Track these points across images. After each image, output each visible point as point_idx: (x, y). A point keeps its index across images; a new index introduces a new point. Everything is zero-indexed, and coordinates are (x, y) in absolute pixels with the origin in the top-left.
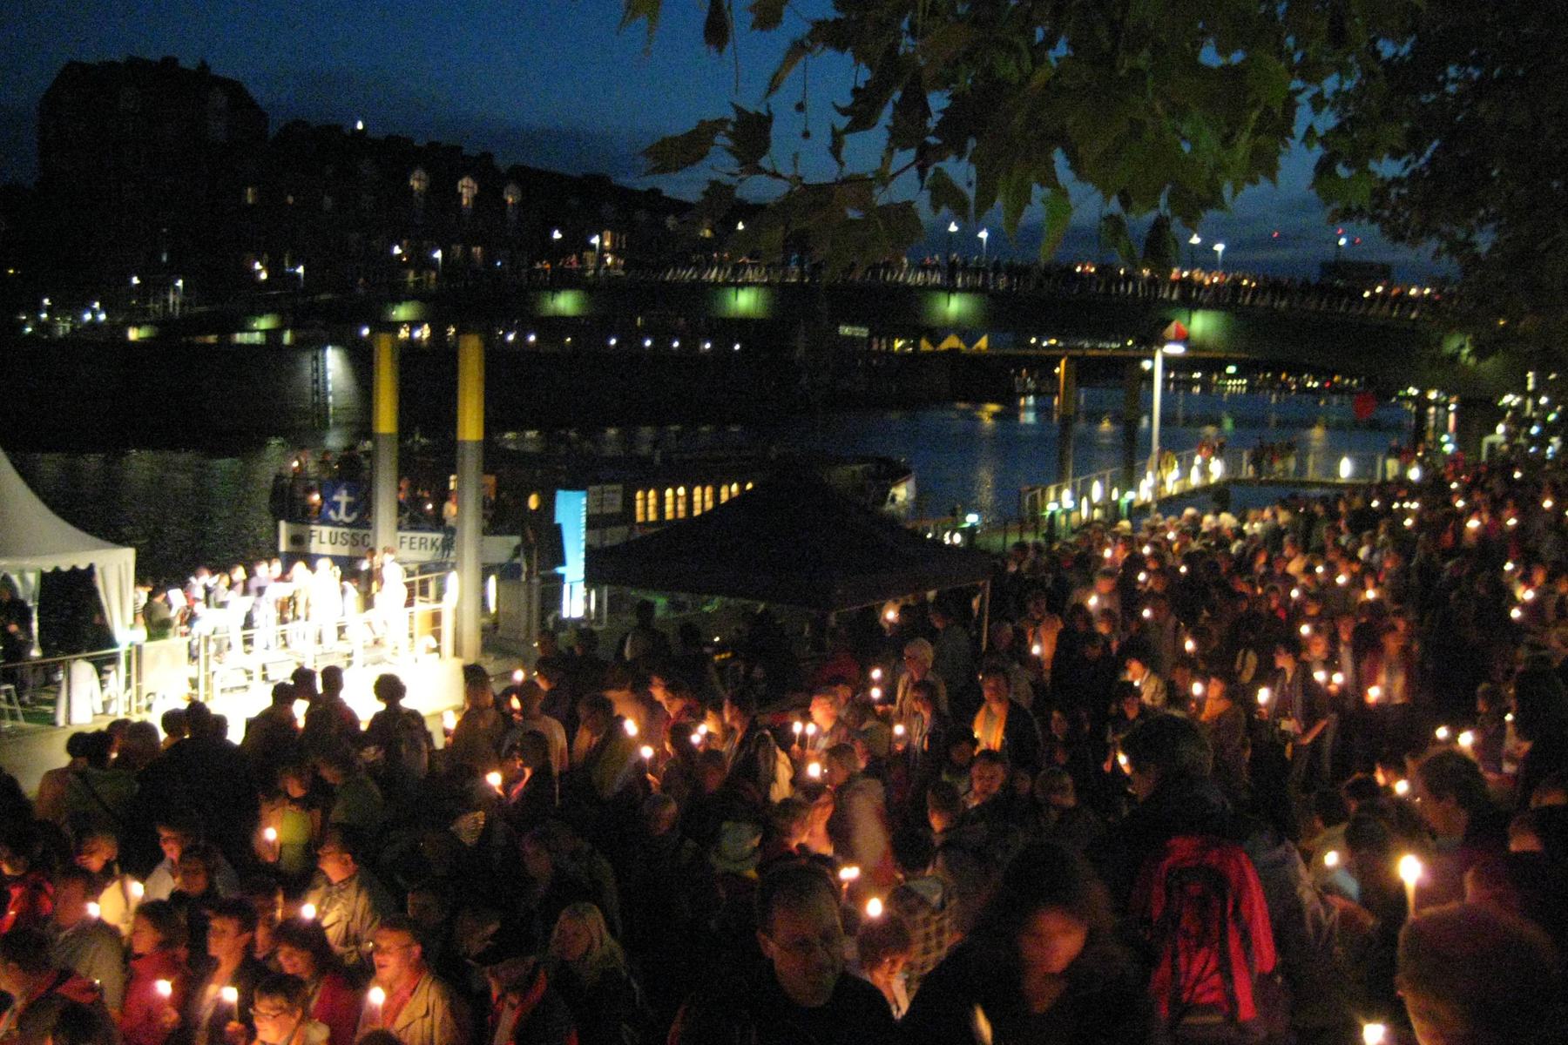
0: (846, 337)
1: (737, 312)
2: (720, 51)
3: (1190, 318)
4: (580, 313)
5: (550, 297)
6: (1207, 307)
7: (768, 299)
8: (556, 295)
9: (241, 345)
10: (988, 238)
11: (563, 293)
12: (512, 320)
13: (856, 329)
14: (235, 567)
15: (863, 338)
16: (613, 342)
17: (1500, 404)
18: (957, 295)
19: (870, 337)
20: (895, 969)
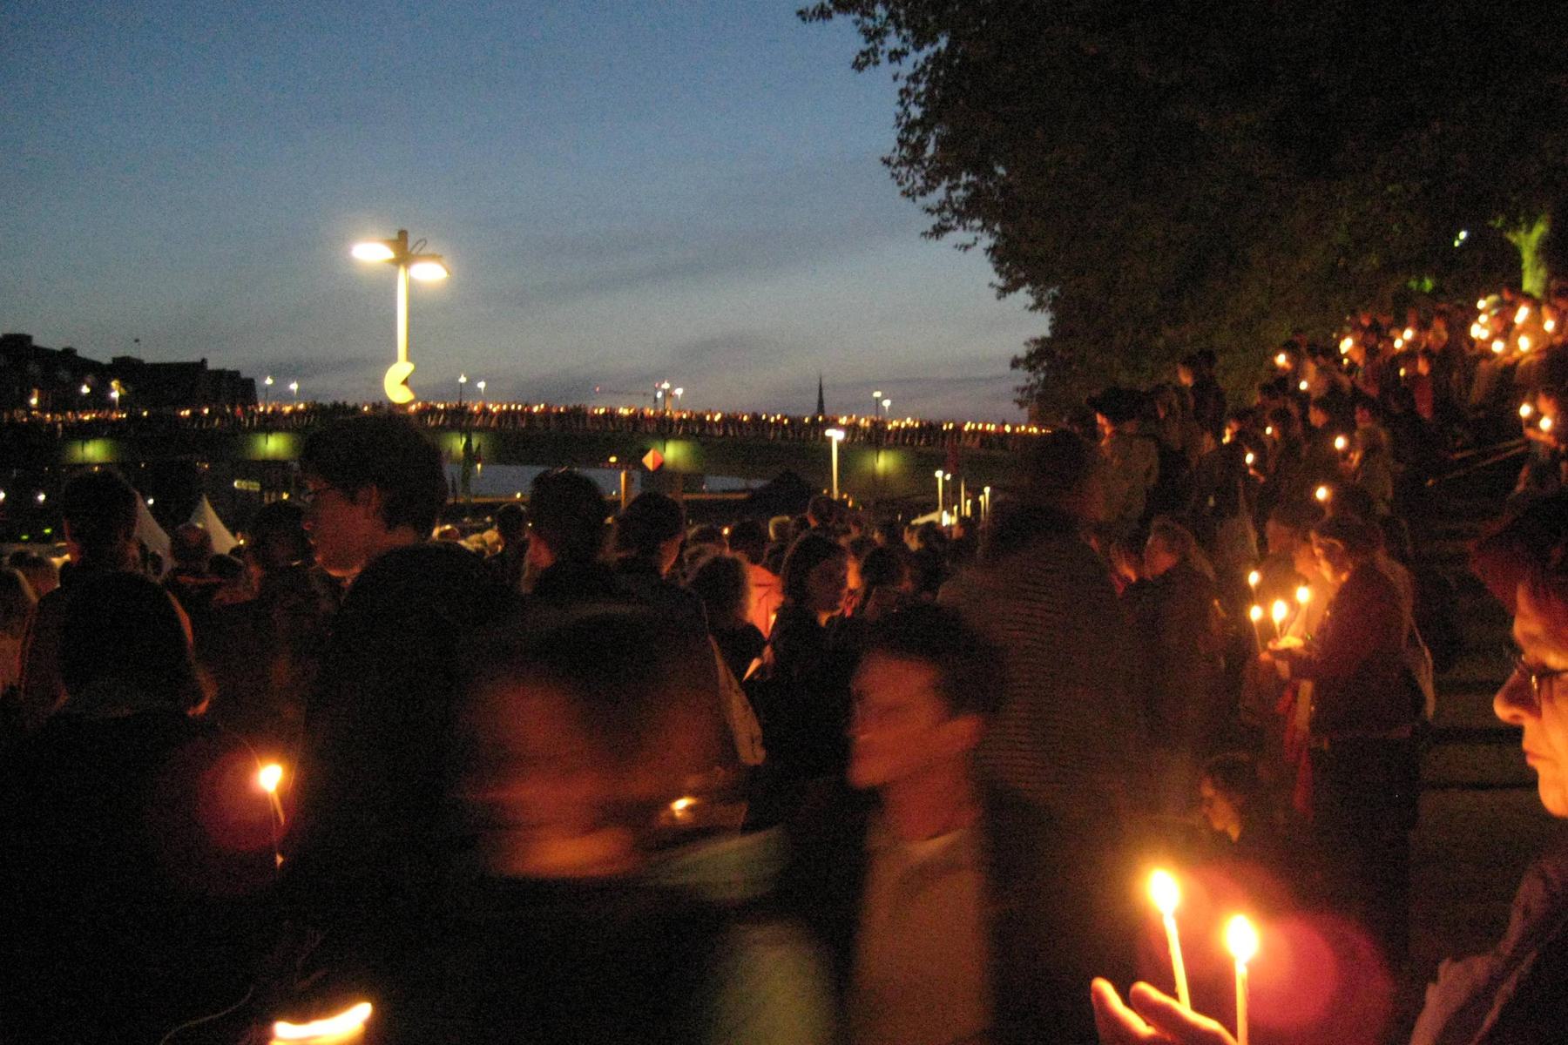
0: (447, 523)
1: (265, 454)
2: (1004, 291)
3: (83, 446)
4: (109, 460)
5: (875, 455)
6: (676, 438)
7: (864, 455)
8: (86, 444)
9: (769, 742)
10: (485, 388)
11: (91, 443)
12: (687, 523)
13: (251, 483)
14: (394, 251)
15: (256, 493)
16: (42, 497)
17: (190, 713)
18: (274, 434)
19: (261, 492)
20: (918, 198)
